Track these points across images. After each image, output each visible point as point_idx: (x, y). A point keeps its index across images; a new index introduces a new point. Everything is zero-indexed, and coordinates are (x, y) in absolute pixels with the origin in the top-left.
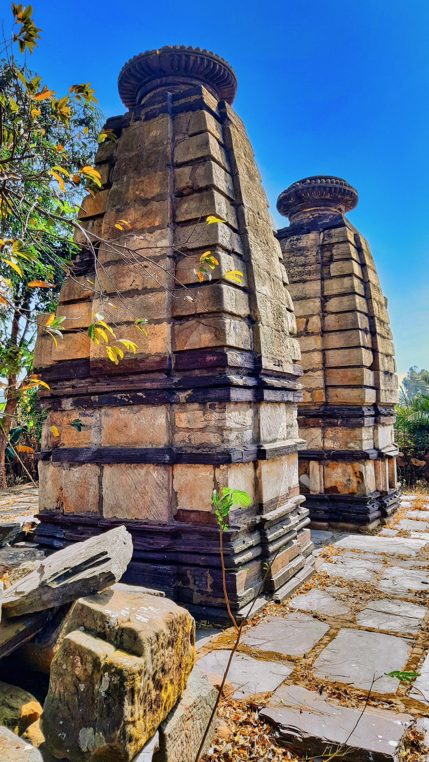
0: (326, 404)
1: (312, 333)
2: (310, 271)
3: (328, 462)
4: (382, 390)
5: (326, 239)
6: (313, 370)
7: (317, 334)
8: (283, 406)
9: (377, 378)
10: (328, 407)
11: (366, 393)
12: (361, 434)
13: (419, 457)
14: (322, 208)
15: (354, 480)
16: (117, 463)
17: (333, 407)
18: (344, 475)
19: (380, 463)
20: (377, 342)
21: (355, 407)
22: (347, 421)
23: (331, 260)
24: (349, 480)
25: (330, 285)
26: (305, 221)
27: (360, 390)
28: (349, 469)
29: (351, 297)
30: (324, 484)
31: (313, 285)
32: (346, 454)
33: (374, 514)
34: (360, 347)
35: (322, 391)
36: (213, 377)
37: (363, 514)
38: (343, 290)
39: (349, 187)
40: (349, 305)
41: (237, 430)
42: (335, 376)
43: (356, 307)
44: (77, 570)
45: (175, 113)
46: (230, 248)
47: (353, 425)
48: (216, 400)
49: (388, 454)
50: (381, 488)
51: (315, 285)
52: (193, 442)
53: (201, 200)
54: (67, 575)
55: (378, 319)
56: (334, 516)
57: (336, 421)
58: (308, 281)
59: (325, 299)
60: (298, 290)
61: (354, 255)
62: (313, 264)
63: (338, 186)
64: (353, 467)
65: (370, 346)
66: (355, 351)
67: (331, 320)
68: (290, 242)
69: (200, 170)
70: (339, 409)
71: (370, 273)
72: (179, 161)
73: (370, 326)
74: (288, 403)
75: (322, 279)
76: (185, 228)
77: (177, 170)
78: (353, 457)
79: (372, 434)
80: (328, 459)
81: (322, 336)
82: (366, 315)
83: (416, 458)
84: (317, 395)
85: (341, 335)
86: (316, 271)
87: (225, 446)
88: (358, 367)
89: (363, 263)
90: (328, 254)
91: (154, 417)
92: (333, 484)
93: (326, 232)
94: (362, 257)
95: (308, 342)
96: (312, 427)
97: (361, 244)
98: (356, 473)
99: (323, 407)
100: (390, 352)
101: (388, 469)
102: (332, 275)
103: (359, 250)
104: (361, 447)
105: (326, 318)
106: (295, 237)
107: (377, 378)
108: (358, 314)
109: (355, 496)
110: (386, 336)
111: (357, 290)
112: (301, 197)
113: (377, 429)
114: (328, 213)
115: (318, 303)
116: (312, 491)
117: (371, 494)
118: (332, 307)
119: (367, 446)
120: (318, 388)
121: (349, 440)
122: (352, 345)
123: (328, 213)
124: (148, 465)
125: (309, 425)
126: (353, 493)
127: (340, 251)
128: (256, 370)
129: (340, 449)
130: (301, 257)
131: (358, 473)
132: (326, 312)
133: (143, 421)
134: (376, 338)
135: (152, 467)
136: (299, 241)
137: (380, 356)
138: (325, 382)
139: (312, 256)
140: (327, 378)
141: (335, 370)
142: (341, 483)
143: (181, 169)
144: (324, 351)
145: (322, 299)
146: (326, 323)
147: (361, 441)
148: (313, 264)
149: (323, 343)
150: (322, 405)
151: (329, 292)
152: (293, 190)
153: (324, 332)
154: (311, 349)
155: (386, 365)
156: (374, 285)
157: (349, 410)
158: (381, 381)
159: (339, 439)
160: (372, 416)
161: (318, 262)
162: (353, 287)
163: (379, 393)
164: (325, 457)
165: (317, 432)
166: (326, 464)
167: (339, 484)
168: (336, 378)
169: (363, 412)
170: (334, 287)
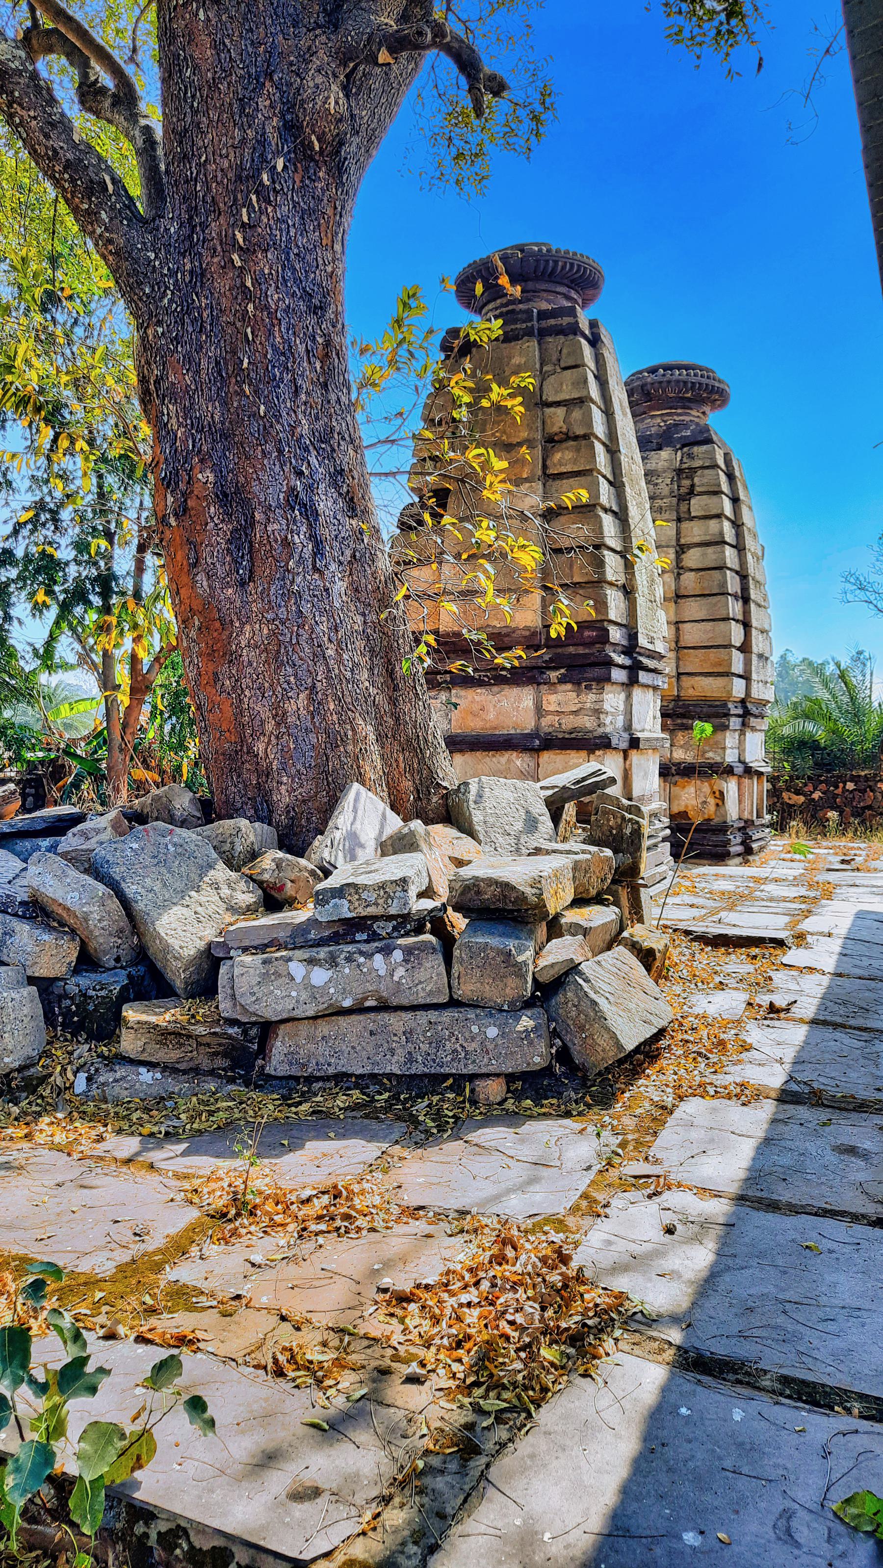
3: (677, 778)
5: (685, 460)
8: (651, 690)
9: (748, 663)
14: (679, 411)
15: (712, 801)
16: (472, 750)
19: (746, 781)
23: (691, 492)
24: (705, 802)
26: (654, 430)
28: (706, 788)
29: (718, 548)
33: (736, 848)
34: (729, 619)
36: (592, 654)
38: (708, 538)
39: (719, 381)
41: (612, 714)
44: (584, 779)
45: (543, 334)
46: (608, 506)
48: (593, 680)
50: (746, 815)
52: (563, 726)
53: (578, 450)
54: (578, 782)
61: (725, 487)
63: (704, 381)
65: (740, 617)
67: (689, 580)
69: (577, 414)
71: (745, 510)
72: (550, 399)
73: (742, 589)
74: (655, 688)
76: (558, 482)
77: (548, 411)
82: (737, 572)
87: (601, 730)
88: (725, 647)
90: (686, 483)
91: (520, 700)
92: (682, 809)
93: (685, 449)
100: (767, 627)
101: (758, 789)
102: (693, 514)
103: (731, 477)
107: (748, 663)
108: (728, 572)
111: (727, 539)
112: (649, 393)
114: (687, 418)
119: (731, 757)
121: (707, 748)
123: (687, 418)
124: (510, 752)
126: (709, 820)
128: (631, 648)
132: (682, 568)
133: (504, 703)
135: (515, 754)
137: (754, 632)
142: (693, 806)
143: (552, 410)
146: (682, 583)
147: (724, 748)
152: (638, 383)
155: (760, 645)
156: (749, 529)
157: (710, 706)
158: (753, 668)
162: (721, 534)
164: (673, 772)
170: (694, 532)
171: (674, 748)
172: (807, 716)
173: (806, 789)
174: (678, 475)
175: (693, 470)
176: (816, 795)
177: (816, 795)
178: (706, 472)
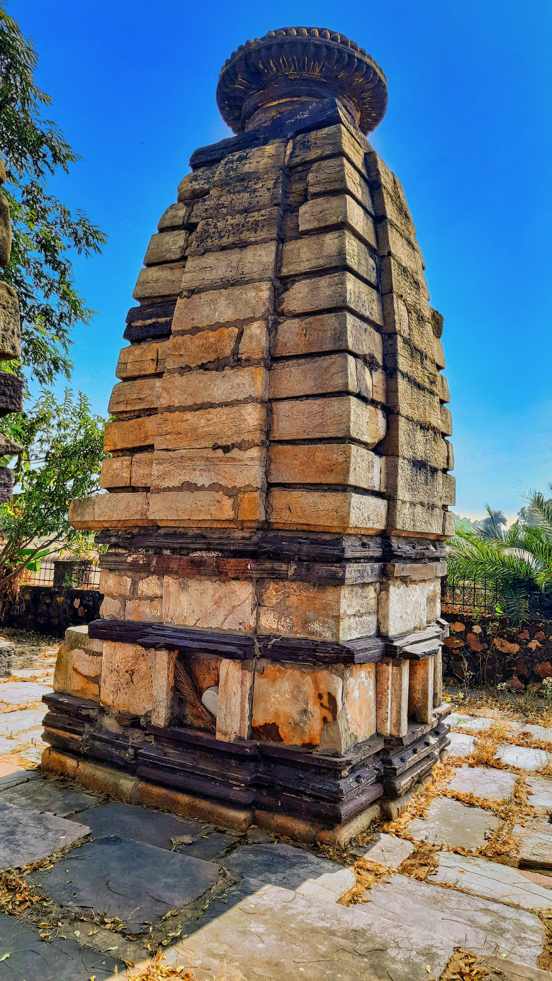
0: (266, 526)
1: (248, 360)
2: (257, 223)
3: (264, 663)
4: (404, 502)
5: (297, 152)
6: (242, 446)
7: (257, 363)
9: (391, 474)
10: (271, 534)
11: (353, 504)
12: (338, 602)
13: (509, 636)
15: (316, 712)
17: (280, 534)
18: (295, 698)
19: (390, 669)
20: (396, 391)
21: (327, 537)
22: (308, 569)
25: (295, 251)
27: (340, 496)
29: (336, 278)
30: (251, 716)
31: (260, 253)
32: (301, 649)
35: (257, 494)
37: (328, 801)
38: (321, 262)
40: (331, 296)
42: (288, 461)
43: (345, 301)
47: (319, 578)
49: (408, 649)
50: (388, 729)
51: (263, 253)
55: (407, 342)
56: (266, 799)
57: (284, 567)
58: (251, 244)
59: (282, 283)
60: (229, 266)
62: (264, 207)
64: (316, 682)
65: (380, 397)
66: (335, 404)
67: (290, 330)
68: (226, 164)
70: (291, 540)
75: (281, 240)
78: (315, 657)
79: (373, 602)
80: (262, 656)
81: (269, 368)
82: (377, 328)
83: (504, 638)
84: (245, 505)
85: (308, 366)
86: (268, 222)
89: (380, 213)
90: (298, 187)
92: (270, 720)
93: (299, 137)
94: (377, 202)
95: (237, 381)
96: (234, 579)
97: (378, 174)
98: (320, 696)
99: (260, 534)
102: (302, 228)
104: (336, 635)
105: (280, 328)
106: (237, 155)
107: (391, 474)
109: (315, 754)
110: (427, 385)
111: (352, 262)
113: (387, 591)
115: (265, 292)
116: (221, 731)
117: (357, 747)
118: (295, 302)
120: (248, 489)
121: (311, 615)
122: (330, 390)
125: (226, 574)
126: (311, 746)
127: (324, 176)
129: (291, 635)
130: (242, 194)
131: (325, 698)
132: (282, 314)
134: (397, 382)
136: (244, 162)
137: (402, 424)
138: (267, 474)
139: (264, 192)
140: (273, 466)
141: (289, 447)
144: (269, 404)
145: (278, 284)
147: (337, 618)
148: (264, 207)
149: (269, 385)
150: (258, 529)
151: (291, 267)
153: (273, 360)
154: (241, 397)
159: (291, 610)
160: (377, 560)
161: (275, 202)
162: (342, 253)
163: (395, 507)
165: (244, 592)
166: (259, 667)
167: (282, 719)
168: (291, 466)
169: (343, 550)
170: (303, 255)
171: (262, 610)
172: (525, 546)
173: (521, 636)
174: (287, 176)
175: (307, 164)
176: (534, 645)
177: (534, 645)
178: (325, 163)
